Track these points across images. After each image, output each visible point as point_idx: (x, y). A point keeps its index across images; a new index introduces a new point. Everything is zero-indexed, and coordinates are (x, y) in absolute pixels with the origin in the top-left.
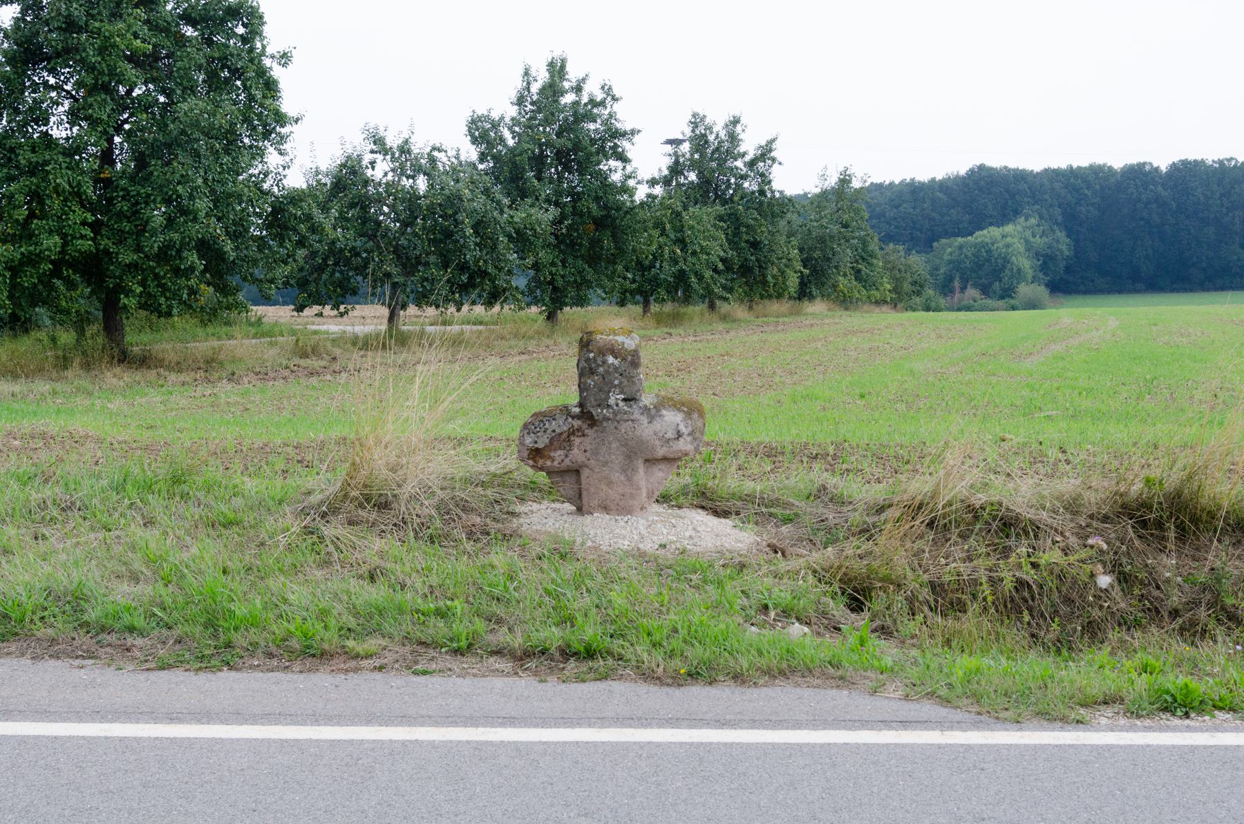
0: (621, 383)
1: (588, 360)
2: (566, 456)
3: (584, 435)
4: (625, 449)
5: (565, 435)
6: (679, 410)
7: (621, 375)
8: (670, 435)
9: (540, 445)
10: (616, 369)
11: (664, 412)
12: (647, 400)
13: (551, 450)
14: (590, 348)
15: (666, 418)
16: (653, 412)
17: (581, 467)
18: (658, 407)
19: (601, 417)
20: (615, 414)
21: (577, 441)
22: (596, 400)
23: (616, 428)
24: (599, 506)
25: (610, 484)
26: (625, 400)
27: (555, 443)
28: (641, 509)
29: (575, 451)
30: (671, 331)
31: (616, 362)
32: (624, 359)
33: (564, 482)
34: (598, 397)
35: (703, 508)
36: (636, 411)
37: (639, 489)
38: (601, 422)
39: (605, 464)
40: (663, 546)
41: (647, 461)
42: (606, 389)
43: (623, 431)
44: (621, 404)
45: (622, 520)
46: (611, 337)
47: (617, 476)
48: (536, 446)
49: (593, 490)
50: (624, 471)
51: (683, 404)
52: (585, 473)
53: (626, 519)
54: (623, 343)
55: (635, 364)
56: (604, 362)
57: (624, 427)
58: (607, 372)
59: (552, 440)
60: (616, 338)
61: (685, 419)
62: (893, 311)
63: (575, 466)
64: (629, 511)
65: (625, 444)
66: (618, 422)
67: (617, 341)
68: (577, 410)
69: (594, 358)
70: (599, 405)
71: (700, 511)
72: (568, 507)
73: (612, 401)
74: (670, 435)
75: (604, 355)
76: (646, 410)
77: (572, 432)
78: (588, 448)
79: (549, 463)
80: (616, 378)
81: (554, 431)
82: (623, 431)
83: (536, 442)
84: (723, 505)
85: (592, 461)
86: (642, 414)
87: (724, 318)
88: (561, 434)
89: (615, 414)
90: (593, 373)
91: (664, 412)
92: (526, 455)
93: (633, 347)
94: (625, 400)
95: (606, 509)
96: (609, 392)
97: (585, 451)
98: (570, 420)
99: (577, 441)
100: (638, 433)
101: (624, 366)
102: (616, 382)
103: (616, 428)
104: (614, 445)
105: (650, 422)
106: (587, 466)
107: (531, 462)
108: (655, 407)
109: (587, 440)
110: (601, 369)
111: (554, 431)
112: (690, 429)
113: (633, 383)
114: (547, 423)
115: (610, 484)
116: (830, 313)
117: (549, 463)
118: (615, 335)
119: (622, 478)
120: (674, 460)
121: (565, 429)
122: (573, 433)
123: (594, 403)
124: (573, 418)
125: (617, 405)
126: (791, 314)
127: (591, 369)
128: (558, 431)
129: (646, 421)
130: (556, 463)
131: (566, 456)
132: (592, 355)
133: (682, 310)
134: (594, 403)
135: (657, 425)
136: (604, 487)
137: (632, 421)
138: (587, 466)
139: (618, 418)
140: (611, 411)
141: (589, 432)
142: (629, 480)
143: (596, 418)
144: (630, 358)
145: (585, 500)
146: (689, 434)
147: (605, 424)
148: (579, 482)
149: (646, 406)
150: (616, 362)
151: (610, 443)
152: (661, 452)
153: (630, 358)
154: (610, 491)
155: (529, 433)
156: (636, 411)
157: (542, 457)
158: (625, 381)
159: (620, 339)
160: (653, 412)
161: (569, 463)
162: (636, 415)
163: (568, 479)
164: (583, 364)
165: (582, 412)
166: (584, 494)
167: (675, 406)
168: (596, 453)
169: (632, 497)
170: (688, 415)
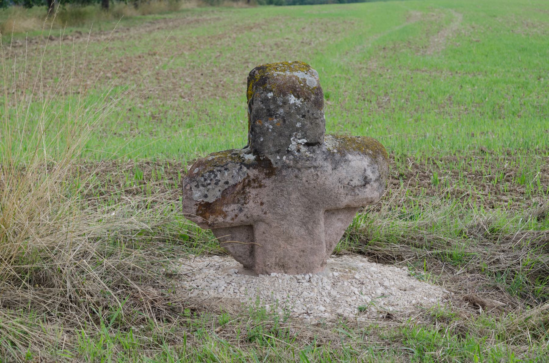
0: (303, 126)
1: (265, 101)
2: (241, 210)
3: (260, 186)
4: (305, 200)
5: (239, 187)
6: (365, 153)
7: (304, 116)
8: (356, 182)
9: (211, 200)
10: (298, 110)
11: (350, 157)
12: (328, 143)
13: (222, 205)
14: (268, 86)
15: (353, 164)
16: (338, 156)
17: (255, 222)
18: (342, 152)
19: (280, 165)
20: (296, 161)
21: (253, 192)
22: (275, 146)
23: (296, 177)
24: (277, 264)
25: (289, 239)
26: (307, 145)
27: (228, 196)
28: (322, 265)
29: (251, 204)
30: (79, 29)
31: (298, 102)
32: (307, 99)
33: (233, 238)
34: (277, 142)
35: (360, 253)
36: (320, 157)
37: (320, 243)
38: (280, 171)
39: (284, 217)
40: (362, 310)
41: (327, 211)
42: (287, 133)
43: (304, 179)
44: (303, 149)
45: (304, 278)
46: (288, 73)
47: (296, 230)
48: (206, 200)
49: (269, 247)
50: (305, 224)
51: (367, 147)
52: (260, 229)
53: (307, 277)
54: (304, 80)
55: (318, 104)
56: (285, 103)
57: (305, 175)
58: (288, 114)
59: (224, 193)
60: (296, 74)
61: (371, 164)
62: (247, 6)
63: (250, 221)
64: (308, 268)
65: (306, 195)
66: (299, 170)
67: (297, 78)
68: (251, 157)
69: (274, 98)
70: (278, 152)
71: (359, 257)
72: (232, 263)
73: (293, 147)
74: (356, 182)
75: (285, 95)
76: (329, 154)
77: (248, 183)
78: (265, 200)
79: (220, 219)
80: (298, 121)
81: (227, 183)
82: (304, 179)
83: (206, 196)
84: (385, 249)
85: (269, 215)
86: (326, 159)
87: (118, 16)
88: (235, 185)
89: (296, 161)
90: (271, 116)
91: (350, 157)
92: (194, 209)
93: (315, 85)
94: (307, 145)
95: (283, 267)
96: (291, 136)
97: (262, 204)
98: (245, 169)
99: (253, 192)
100: (320, 181)
101: (308, 106)
102: (298, 125)
103: (296, 177)
104: (294, 196)
105: (334, 169)
106: (262, 221)
107: (200, 219)
108: (339, 151)
109: (264, 191)
110: (281, 111)
111: (227, 183)
112: (377, 174)
113: (317, 125)
114: (219, 174)
115: (289, 239)
116: (199, 9)
117: (220, 219)
118: (292, 70)
119: (303, 232)
120: (355, 208)
121: (240, 179)
122: (249, 185)
123: (273, 149)
124: (248, 166)
125: (299, 151)
126: (171, 11)
127: (269, 110)
128: (232, 182)
129: (330, 167)
130: (228, 219)
131: (241, 210)
132: (270, 95)
133: (83, 9)
134: (273, 149)
135: (343, 172)
136: (282, 243)
137: (315, 167)
138: (262, 221)
139: (299, 165)
140: (291, 157)
141: (267, 182)
142: (310, 233)
143: (275, 166)
144: (313, 97)
145: (259, 259)
146: (377, 180)
147: (284, 173)
148: (251, 237)
149: (329, 150)
150: (298, 102)
151: (289, 194)
152: (345, 201)
153: (313, 97)
154: (289, 247)
155: (197, 186)
156: (320, 157)
157: (212, 213)
158: (307, 123)
159: (300, 75)
160: (338, 156)
161: (244, 218)
162: (320, 162)
163: (238, 235)
164: (258, 105)
165: (258, 159)
166: (259, 252)
167: (359, 149)
168: (273, 205)
169: (314, 252)
170: (374, 158)
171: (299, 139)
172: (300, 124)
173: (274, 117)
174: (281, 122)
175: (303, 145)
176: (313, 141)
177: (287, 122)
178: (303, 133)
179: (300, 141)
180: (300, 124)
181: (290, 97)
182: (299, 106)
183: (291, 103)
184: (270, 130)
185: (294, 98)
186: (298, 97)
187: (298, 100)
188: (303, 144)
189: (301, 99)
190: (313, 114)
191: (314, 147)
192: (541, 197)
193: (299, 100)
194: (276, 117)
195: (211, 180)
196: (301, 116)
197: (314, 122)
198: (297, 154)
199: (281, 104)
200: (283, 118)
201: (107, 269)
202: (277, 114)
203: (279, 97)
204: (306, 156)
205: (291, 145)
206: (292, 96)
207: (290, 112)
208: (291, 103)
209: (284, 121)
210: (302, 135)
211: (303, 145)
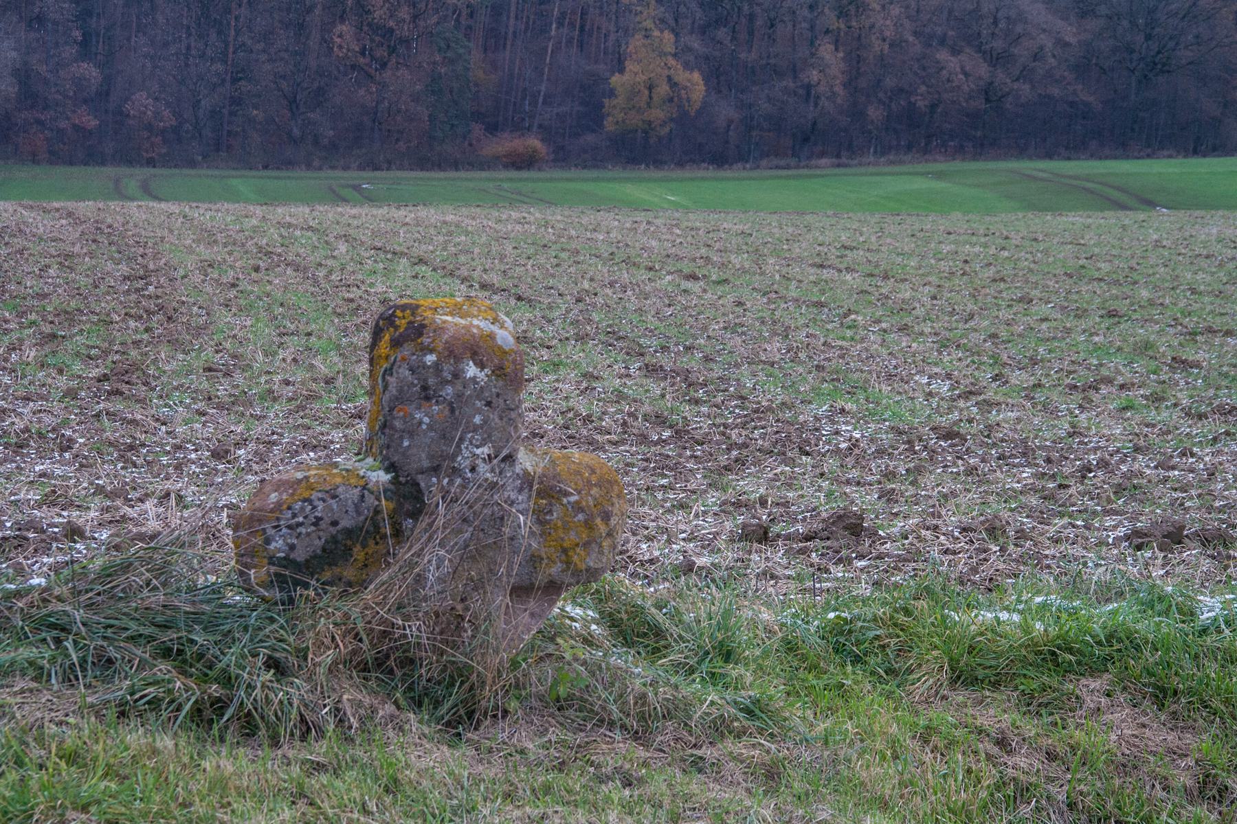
0: (485, 421)
7: (489, 404)
75: (458, 359)
80: (479, 411)
174: (447, 412)
179: (478, 451)
181: (468, 365)
185: (474, 368)
186: (481, 366)
190: (505, 401)
194: (437, 401)
195: (305, 517)
196: (483, 402)
202: (441, 396)
206: (471, 363)
209: (452, 411)
210: (484, 439)
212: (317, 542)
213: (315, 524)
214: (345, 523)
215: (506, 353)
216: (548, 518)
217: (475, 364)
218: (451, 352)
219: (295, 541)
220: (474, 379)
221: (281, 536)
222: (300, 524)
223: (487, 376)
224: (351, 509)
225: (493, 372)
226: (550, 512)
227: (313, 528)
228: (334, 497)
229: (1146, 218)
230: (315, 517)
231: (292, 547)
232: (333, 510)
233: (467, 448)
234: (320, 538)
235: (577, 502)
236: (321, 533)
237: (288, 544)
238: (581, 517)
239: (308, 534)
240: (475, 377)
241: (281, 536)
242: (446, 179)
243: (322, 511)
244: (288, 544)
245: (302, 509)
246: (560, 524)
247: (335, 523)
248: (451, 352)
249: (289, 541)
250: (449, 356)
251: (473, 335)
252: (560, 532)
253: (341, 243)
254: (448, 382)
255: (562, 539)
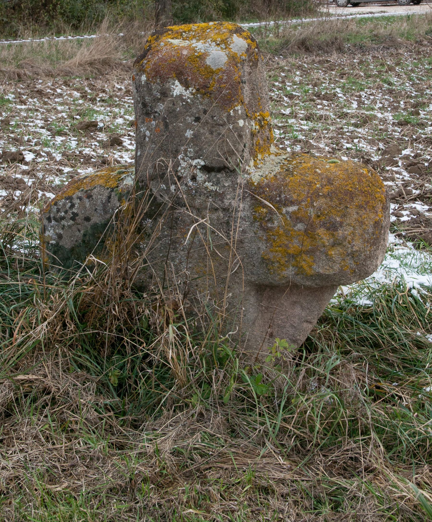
0: (196, 136)
7: (197, 119)
26: (206, 169)
44: (201, 177)
58: (171, 112)
75: (164, 79)
80: (189, 126)
94: (206, 169)
125: (194, 178)
150: (187, 94)
171: (193, 159)
172: (192, 132)
173: (152, 117)
174: (162, 127)
175: (200, 169)
176: (214, 165)
177: (170, 127)
178: (197, 149)
179: (194, 163)
180: (192, 132)
181: (174, 84)
182: (189, 100)
183: (175, 94)
184: (147, 139)
185: (180, 86)
186: (186, 85)
187: (186, 90)
188: (199, 167)
189: (190, 89)
190: (213, 117)
191: (219, 175)
192: (419, 53)
193: (188, 91)
194: (154, 117)
195: (66, 212)
196: (193, 118)
197: (216, 131)
198: (191, 183)
199: (159, 95)
200: (164, 119)
201: (399, 452)
202: (156, 112)
203: (154, 83)
204: (206, 188)
205: (180, 168)
206: (177, 82)
207: (174, 110)
208: (175, 94)
209: (166, 125)
210: (196, 152)
211: (200, 169)
212: (77, 233)
213: (73, 219)
214: (96, 219)
215: (212, 72)
216: (269, 225)
217: (181, 83)
218: (156, 72)
219: (61, 232)
220: (180, 96)
221: (51, 227)
222: (63, 218)
223: (192, 94)
224: (100, 208)
225: (198, 90)
226: (271, 220)
227: (71, 222)
228: (89, 197)
229: (426, 513)
230: (73, 213)
231: (60, 236)
232: (86, 208)
233: (183, 159)
234: (79, 231)
235: (294, 213)
236: (79, 227)
237: (57, 234)
238: (300, 226)
239: (70, 227)
240: (181, 95)
241: (51, 227)
242: (374, 13)
243: (78, 208)
244: (57, 234)
245: (64, 205)
246: (281, 231)
247: (87, 219)
248: (156, 72)
249: (57, 231)
250: (156, 76)
251: (180, 58)
252: (284, 238)
253: (234, 28)
254: (159, 100)
255: (286, 246)
